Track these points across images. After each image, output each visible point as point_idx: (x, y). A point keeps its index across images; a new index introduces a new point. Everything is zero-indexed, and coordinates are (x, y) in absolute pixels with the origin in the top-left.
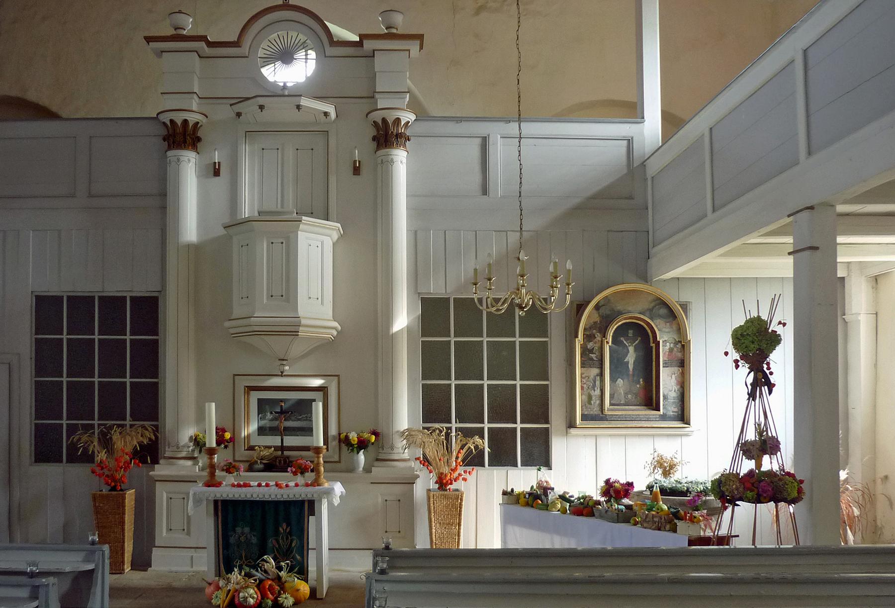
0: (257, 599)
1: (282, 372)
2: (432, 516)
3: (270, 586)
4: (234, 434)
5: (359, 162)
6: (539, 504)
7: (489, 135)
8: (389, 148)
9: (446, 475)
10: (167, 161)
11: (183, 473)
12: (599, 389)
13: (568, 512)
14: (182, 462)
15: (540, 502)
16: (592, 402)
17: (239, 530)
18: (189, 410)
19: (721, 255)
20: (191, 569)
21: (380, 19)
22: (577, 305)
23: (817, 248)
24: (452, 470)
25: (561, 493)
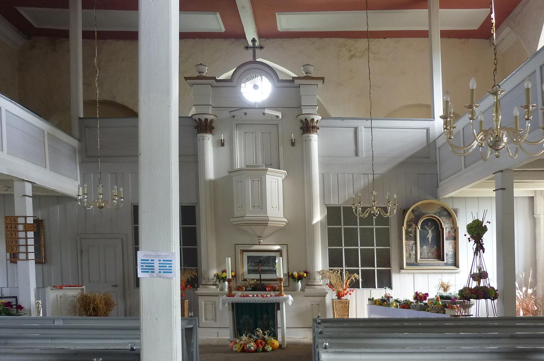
0: (255, 347)
1: (259, 243)
2: (335, 312)
3: (260, 342)
4: (236, 273)
5: (294, 140)
6: (386, 304)
7: (358, 127)
8: (309, 133)
9: (341, 292)
10: (197, 139)
11: (211, 292)
12: (414, 251)
13: (399, 307)
14: (211, 287)
15: (386, 303)
16: (411, 257)
17: (244, 317)
18: (213, 261)
19: (471, 187)
20: (217, 338)
21: (302, 68)
22: (403, 210)
23: (504, 189)
24: (344, 289)
25: (396, 299)
